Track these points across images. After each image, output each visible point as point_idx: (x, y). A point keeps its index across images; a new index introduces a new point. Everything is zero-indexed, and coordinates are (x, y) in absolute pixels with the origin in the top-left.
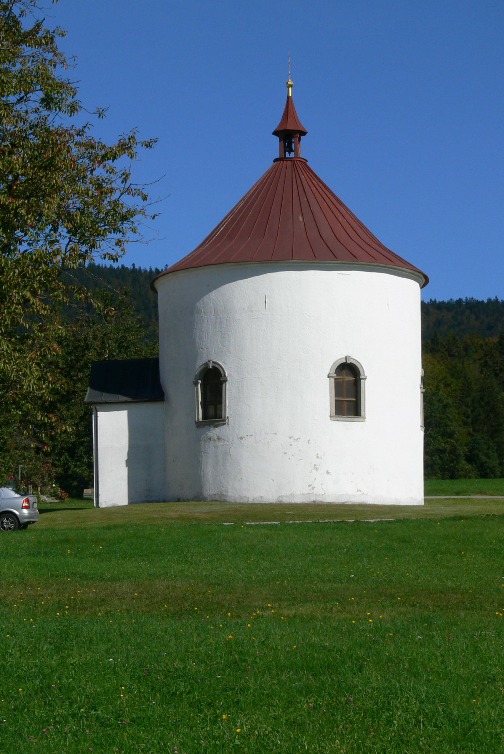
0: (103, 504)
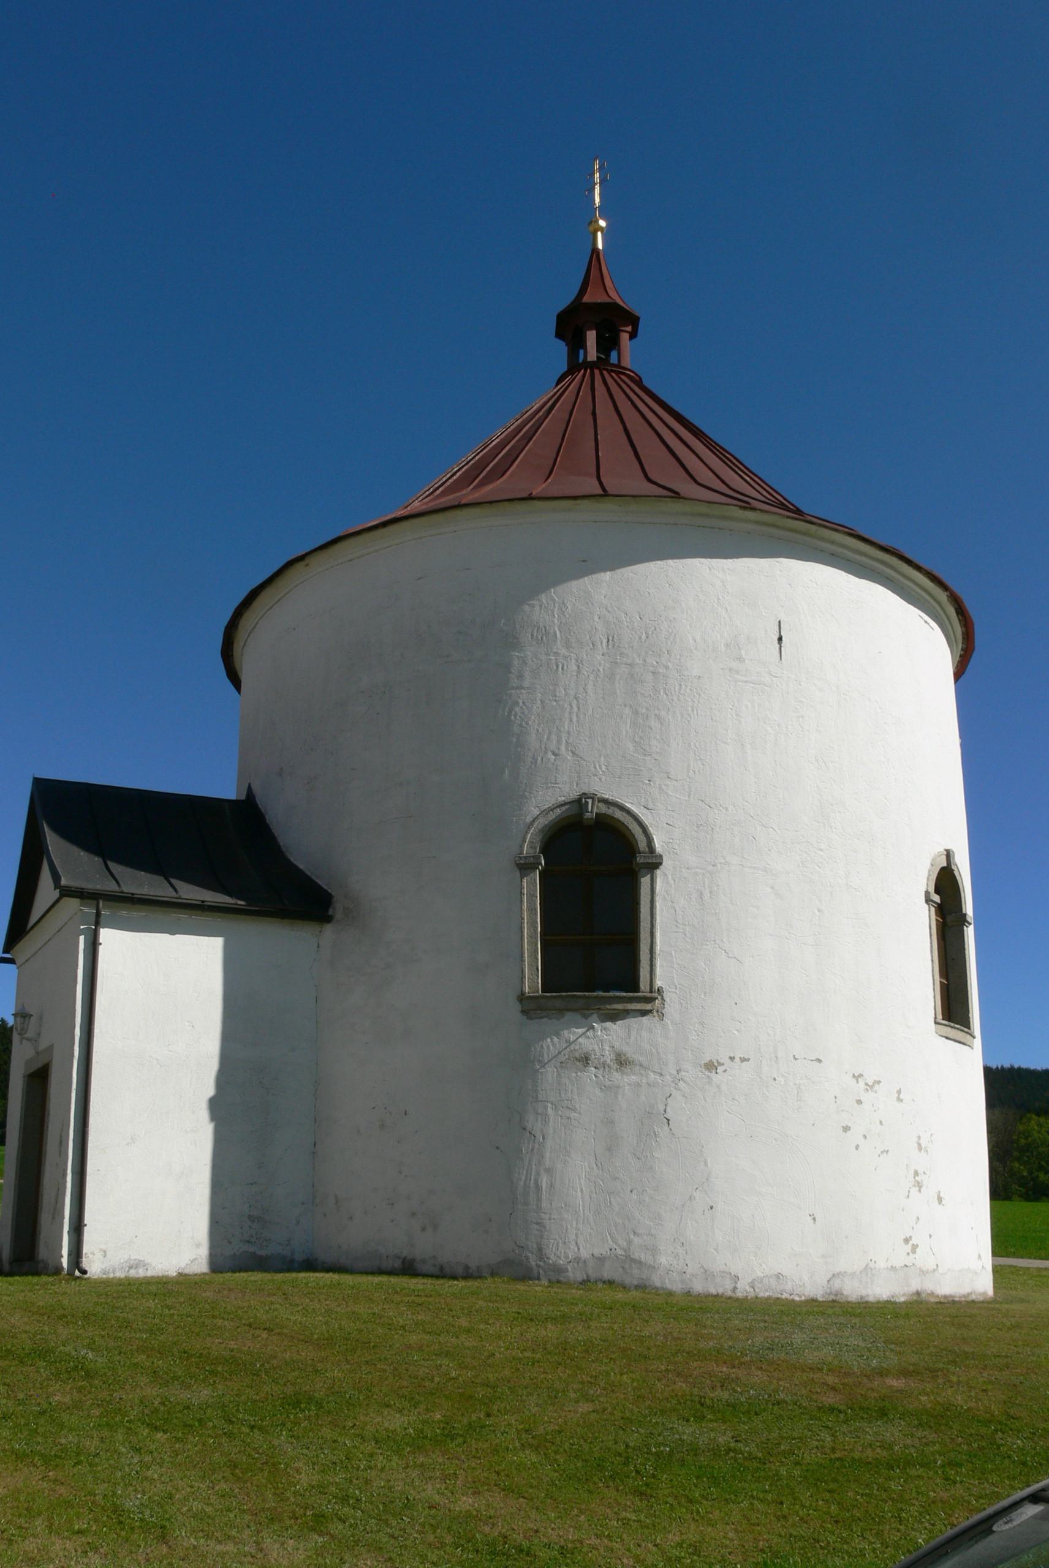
0: (95, 1264)
